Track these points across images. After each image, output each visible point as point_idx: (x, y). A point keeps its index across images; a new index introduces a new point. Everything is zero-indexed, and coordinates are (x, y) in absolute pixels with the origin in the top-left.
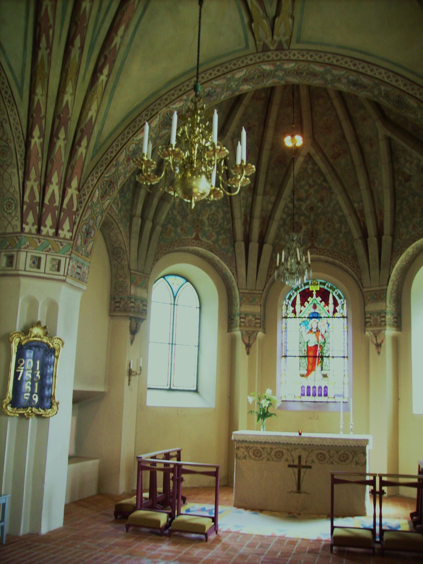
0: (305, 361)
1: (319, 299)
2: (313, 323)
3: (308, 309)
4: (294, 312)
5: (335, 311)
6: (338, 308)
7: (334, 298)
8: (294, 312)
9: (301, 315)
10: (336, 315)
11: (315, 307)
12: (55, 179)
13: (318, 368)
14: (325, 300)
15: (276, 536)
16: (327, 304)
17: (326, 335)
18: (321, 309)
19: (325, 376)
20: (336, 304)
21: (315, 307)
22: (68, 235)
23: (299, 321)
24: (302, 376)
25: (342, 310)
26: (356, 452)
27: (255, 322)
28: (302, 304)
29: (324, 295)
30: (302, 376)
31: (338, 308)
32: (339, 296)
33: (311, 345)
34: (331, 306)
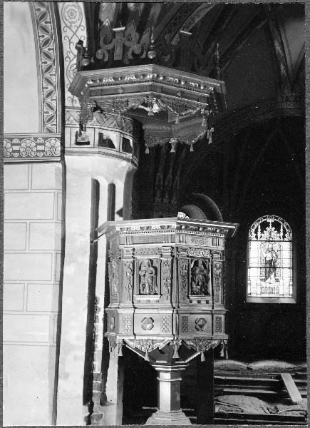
0: (263, 270)
1: (274, 228)
2: (270, 245)
3: (266, 234)
4: (257, 237)
5: (284, 237)
6: (286, 235)
7: (283, 227)
8: (257, 237)
9: (261, 239)
10: (285, 239)
11: (270, 233)
12: (160, 169)
13: (272, 276)
14: (278, 229)
15: (190, 419)
16: (279, 232)
17: (278, 253)
18: (274, 233)
19: (277, 280)
20: (285, 232)
21: (270, 233)
22: (175, 202)
23: (260, 243)
24: (261, 280)
25: (289, 236)
26: (119, 357)
27: (11, 150)
28: (262, 232)
29: (276, 226)
30: (261, 280)
31: (286, 235)
32: (287, 227)
33: (268, 259)
34: (282, 234)
